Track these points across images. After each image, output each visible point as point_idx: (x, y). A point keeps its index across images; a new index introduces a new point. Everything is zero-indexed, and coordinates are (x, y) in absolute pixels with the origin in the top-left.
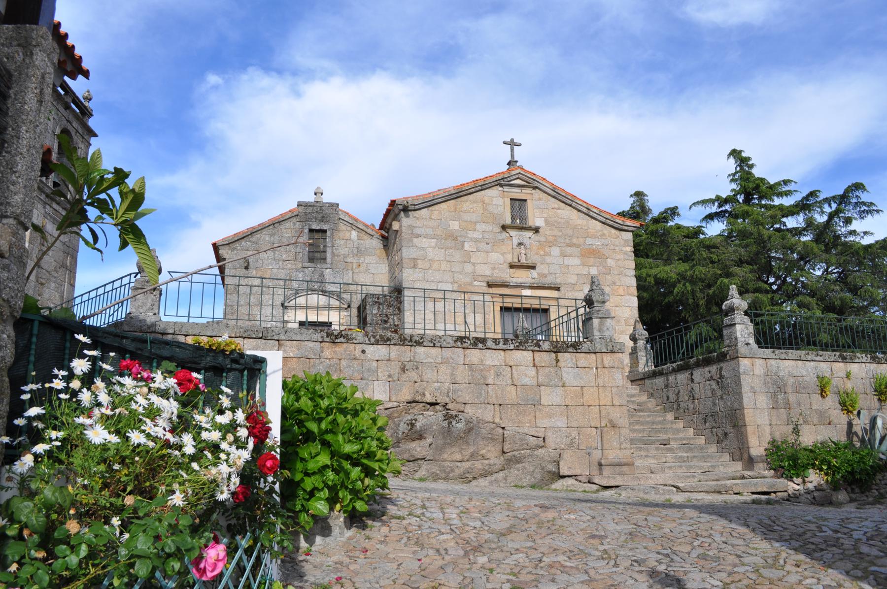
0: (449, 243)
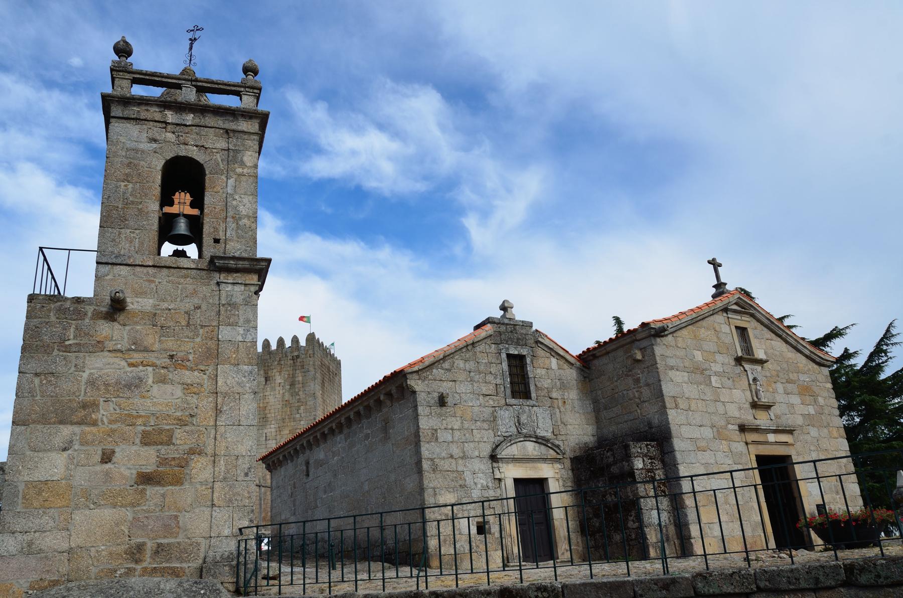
0: (699, 378)
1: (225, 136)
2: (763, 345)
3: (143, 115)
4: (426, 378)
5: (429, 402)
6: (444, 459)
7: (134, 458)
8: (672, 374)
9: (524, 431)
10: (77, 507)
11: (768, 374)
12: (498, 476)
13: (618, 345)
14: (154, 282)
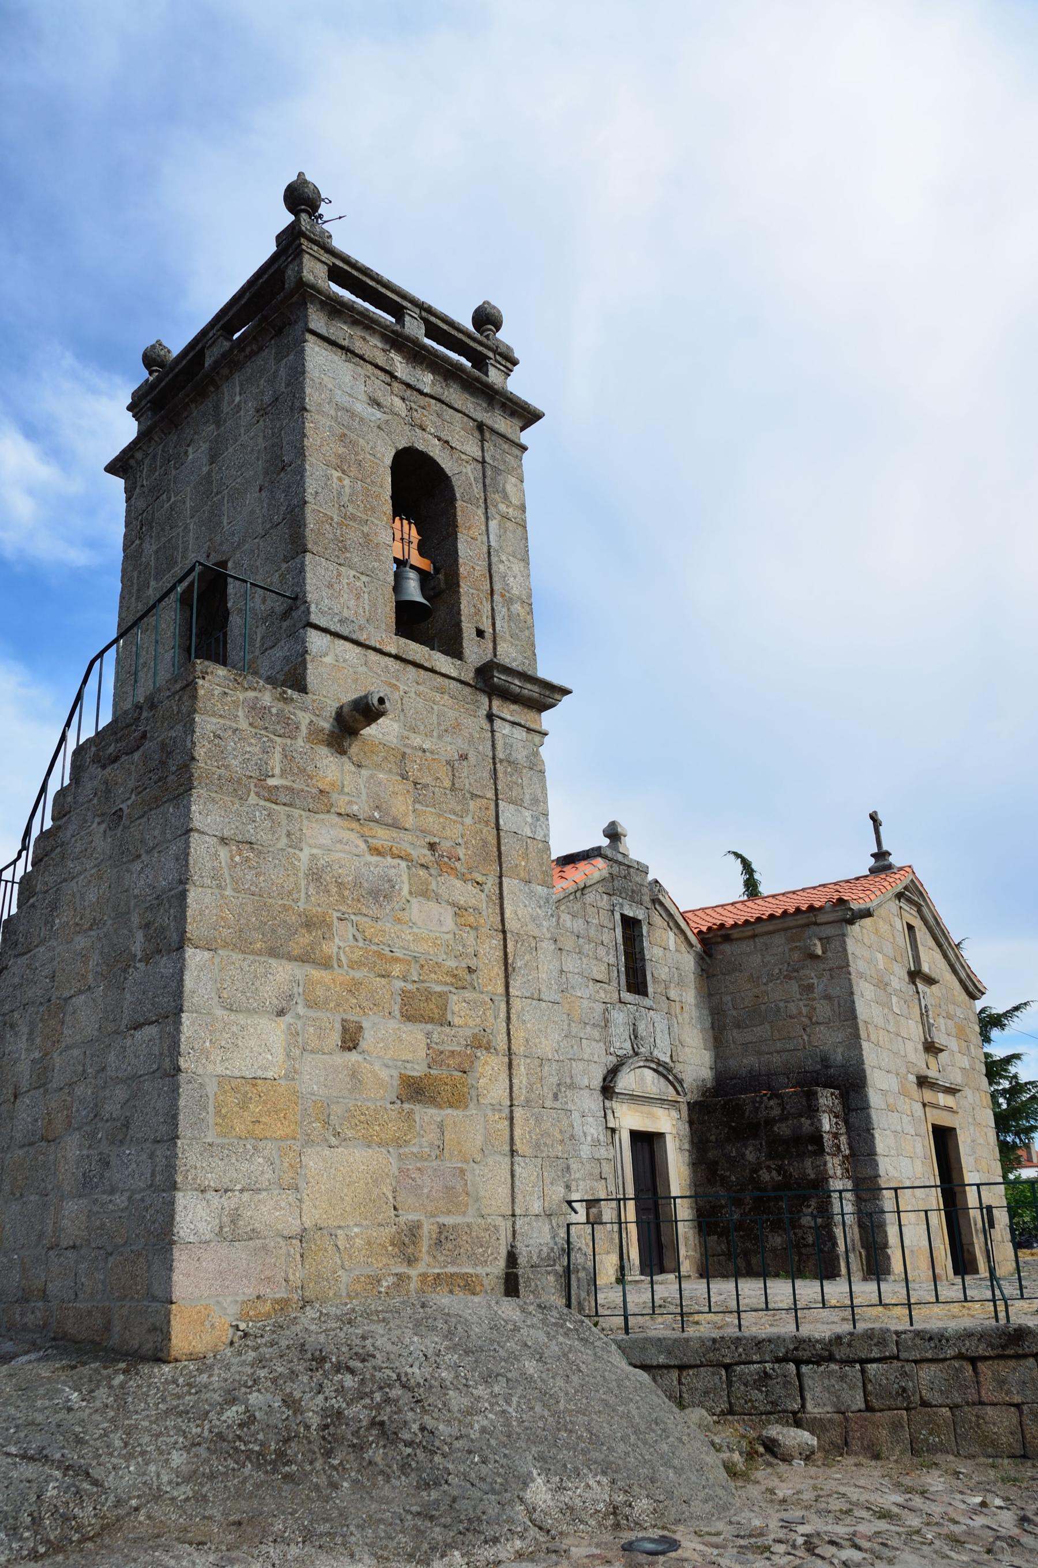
1: (477, 434)
3: (359, 346)
7: (396, 1046)
10: (309, 1142)
12: (611, 1125)
13: (779, 926)
14: (398, 688)
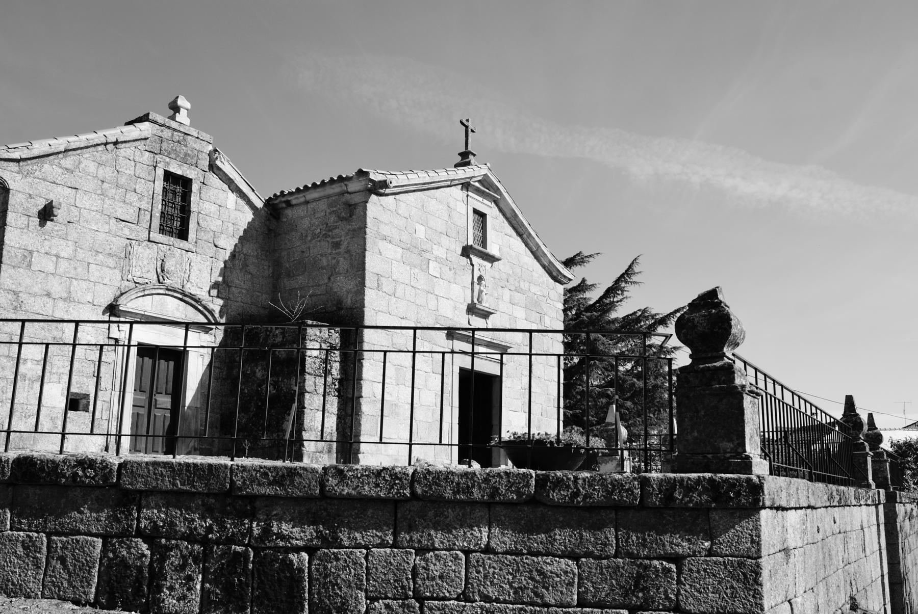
2: (500, 237)
4: (29, 174)
5: (28, 209)
6: (35, 295)
8: (382, 245)
9: (167, 282)
11: (497, 276)
